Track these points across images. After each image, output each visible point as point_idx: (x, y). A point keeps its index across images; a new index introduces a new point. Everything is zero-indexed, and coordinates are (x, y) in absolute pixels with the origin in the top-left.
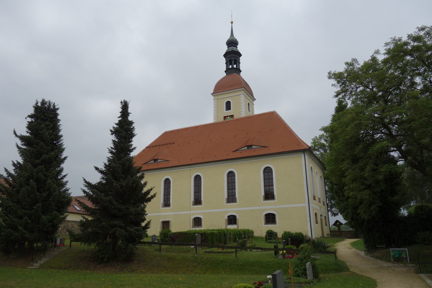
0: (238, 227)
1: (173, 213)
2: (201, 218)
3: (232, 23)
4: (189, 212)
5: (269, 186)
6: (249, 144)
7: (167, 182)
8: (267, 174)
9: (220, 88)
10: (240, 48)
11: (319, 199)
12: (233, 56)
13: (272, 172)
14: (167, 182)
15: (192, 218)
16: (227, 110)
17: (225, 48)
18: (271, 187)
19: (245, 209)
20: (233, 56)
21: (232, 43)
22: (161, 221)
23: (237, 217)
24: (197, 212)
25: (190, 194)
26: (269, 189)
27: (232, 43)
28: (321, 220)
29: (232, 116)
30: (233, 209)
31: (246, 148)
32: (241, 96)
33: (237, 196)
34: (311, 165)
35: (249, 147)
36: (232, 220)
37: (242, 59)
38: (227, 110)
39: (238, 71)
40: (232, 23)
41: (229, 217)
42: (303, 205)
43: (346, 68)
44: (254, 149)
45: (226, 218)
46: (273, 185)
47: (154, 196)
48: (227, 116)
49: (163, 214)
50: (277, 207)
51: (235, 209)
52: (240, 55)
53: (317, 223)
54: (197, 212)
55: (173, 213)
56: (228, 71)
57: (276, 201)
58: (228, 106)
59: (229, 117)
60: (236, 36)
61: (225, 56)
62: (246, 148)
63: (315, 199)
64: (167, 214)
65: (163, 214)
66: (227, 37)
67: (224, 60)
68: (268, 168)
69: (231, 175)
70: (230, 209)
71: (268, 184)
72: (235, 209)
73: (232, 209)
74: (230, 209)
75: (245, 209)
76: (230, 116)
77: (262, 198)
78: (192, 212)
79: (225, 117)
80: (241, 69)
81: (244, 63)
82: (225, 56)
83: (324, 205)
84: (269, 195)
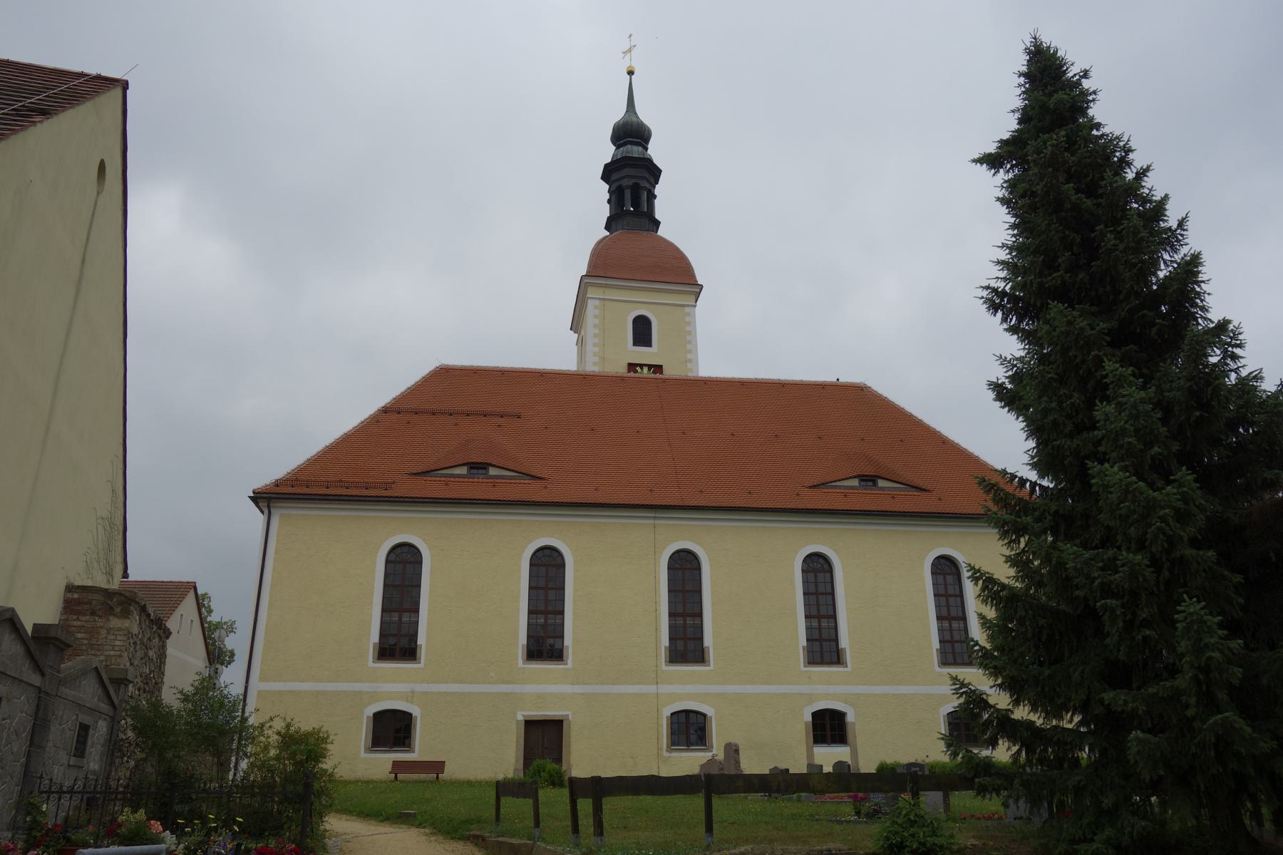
0: (854, 754)
1: (578, 689)
2: (704, 715)
3: (631, 73)
4: (652, 689)
5: (401, 611)
6: (869, 471)
9: (604, 268)
10: (656, 151)
12: (631, 177)
15: (667, 712)
18: (405, 618)
19: (877, 690)
20: (631, 177)
21: (631, 134)
22: (520, 717)
23: (850, 718)
24: (689, 688)
25: (657, 618)
27: (631, 134)
29: (658, 369)
31: (855, 482)
35: (478, 467)
40: (631, 73)
41: (379, 716)
44: (883, 489)
48: (641, 366)
49: (530, 688)
51: (840, 689)
52: (655, 173)
54: (689, 688)
55: (578, 689)
57: (712, 667)
59: (646, 369)
60: (645, 115)
64: (551, 688)
65: (530, 688)
66: (618, 113)
68: (555, 554)
69: (404, 563)
70: (820, 689)
72: (840, 689)
73: (687, 688)
74: (820, 689)
75: (877, 690)
76: (650, 366)
77: (371, 653)
78: (665, 689)
79: (632, 367)
80: (658, 216)
81: (668, 203)
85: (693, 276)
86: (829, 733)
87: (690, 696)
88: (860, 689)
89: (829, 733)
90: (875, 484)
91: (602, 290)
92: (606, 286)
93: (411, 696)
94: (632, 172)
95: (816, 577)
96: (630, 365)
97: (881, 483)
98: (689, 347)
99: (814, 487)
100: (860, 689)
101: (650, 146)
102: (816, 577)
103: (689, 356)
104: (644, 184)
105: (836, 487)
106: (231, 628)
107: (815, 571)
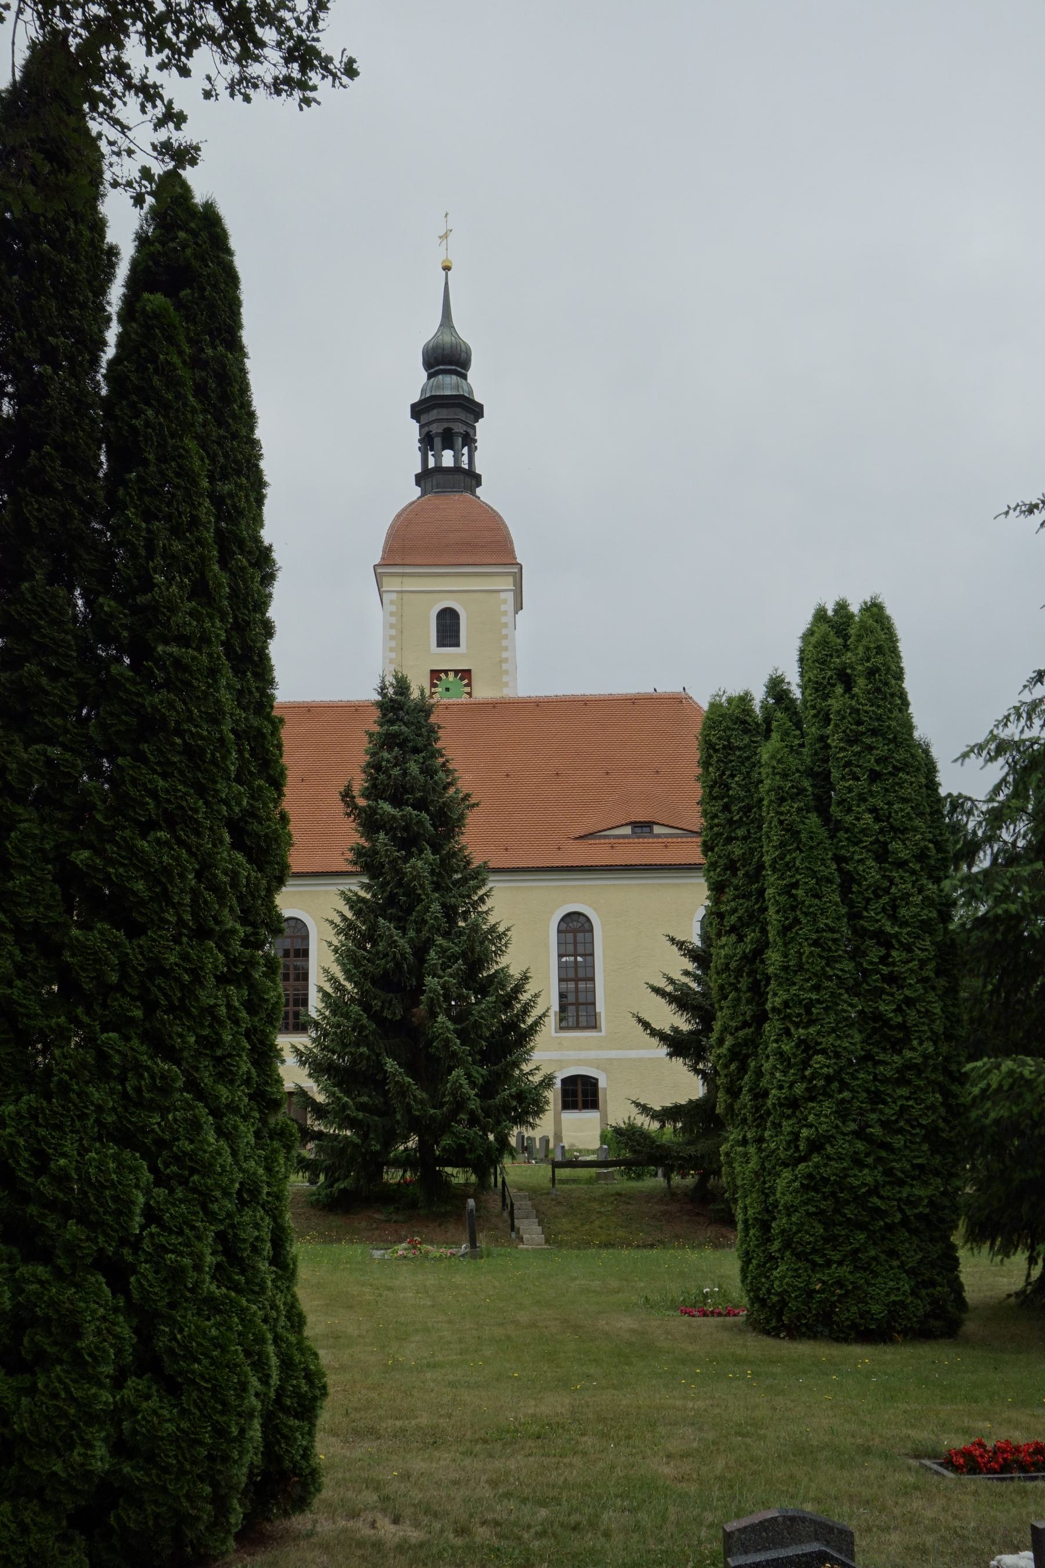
3: (447, 268)
7: (575, 929)
10: (479, 383)
14: (575, 929)
16: (441, 643)
17: (414, 382)
21: (446, 359)
26: (577, 990)
27: (446, 359)
30: (583, 1055)
32: (503, 595)
33: (600, 1007)
35: (642, 827)
38: (441, 643)
40: (447, 268)
44: (658, 836)
46: (592, 979)
48: (446, 672)
52: (476, 411)
58: (448, 628)
59: (451, 675)
60: (466, 331)
61: (418, 411)
62: (627, 830)
66: (427, 330)
67: (413, 429)
70: (572, 1054)
71: (571, 975)
72: (593, 1054)
74: (572, 1054)
76: (456, 672)
81: (492, 449)
82: (418, 411)
85: (511, 552)
86: (580, 1099)
87: (579, 1062)
88: (613, 1054)
89: (580, 1099)
90: (651, 831)
91: (399, 580)
92: (403, 575)
93: (598, 1064)
94: (444, 413)
95: (575, 937)
96: (433, 672)
97: (657, 830)
98: (504, 643)
99: (581, 837)
100: (613, 1054)
101: (471, 374)
102: (575, 937)
103: (505, 655)
104: (459, 428)
105: (606, 837)
106: (178, 128)
107: (575, 932)
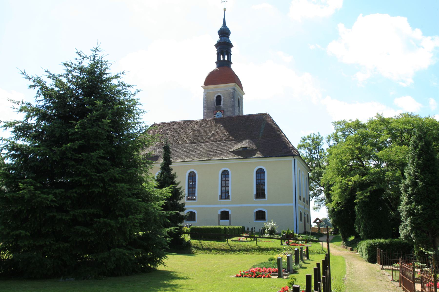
2: (194, 213)
3: (225, 10)
8: (260, 174)
9: (211, 80)
10: (232, 38)
11: (304, 199)
12: (224, 46)
13: (264, 173)
17: (217, 38)
20: (224, 46)
21: (224, 33)
23: (230, 213)
27: (224, 33)
28: (305, 217)
34: (299, 169)
36: (225, 215)
37: (233, 51)
39: (229, 62)
40: (225, 10)
42: (291, 205)
43: (397, 275)
45: (220, 213)
47: (182, 197)
50: (268, 205)
52: (231, 46)
53: (301, 220)
56: (219, 63)
63: (300, 199)
66: (220, 25)
67: (215, 51)
77: (254, 197)
82: (216, 46)
83: (304, 202)
84: (260, 193)
